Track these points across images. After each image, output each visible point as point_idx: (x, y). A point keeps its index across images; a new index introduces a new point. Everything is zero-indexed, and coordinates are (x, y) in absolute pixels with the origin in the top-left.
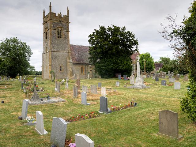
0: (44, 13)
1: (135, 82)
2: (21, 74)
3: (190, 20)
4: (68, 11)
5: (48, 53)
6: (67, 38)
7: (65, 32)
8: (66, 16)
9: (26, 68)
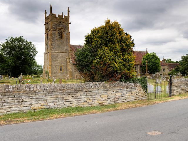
0: (46, 13)
1: (2, 103)
2: (25, 73)
3: (9, 75)
4: (69, 11)
5: (49, 54)
6: (67, 39)
7: (66, 33)
8: (67, 17)
9: (30, 67)
